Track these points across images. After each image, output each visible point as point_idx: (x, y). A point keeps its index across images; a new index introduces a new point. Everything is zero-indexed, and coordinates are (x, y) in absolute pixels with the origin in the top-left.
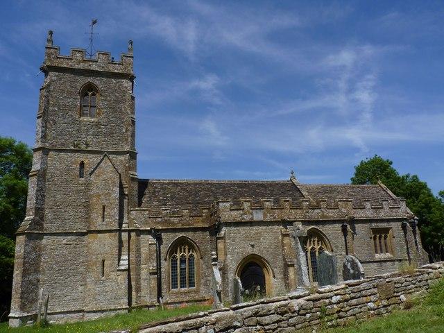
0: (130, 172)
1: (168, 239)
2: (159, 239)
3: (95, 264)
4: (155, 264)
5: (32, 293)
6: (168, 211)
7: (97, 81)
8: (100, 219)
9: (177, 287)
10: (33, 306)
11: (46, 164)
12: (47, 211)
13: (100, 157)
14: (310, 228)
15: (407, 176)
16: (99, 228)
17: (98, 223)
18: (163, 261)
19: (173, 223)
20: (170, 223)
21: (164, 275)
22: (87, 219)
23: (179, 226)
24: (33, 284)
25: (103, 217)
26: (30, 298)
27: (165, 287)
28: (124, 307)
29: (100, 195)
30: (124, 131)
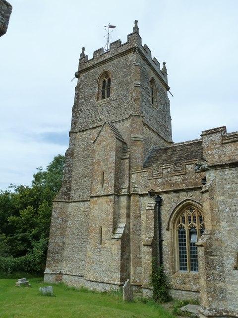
0: (132, 135)
1: (170, 203)
2: (159, 203)
3: (94, 230)
4: (152, 235)
5: (58, 253)
6: (169, 170)
7: (109, 67)
8: (100, 185)
9: (186, 269)
10: (59, 265)
11: (74, 144)
12: (73, 182)
13: (99, 129)
14: (132, 267)
15: (33, 182)
16: (98, 194)
17: (98, 189)
18: (164, 232)
19: (175, 184)
20: (171, 184)
21: (166, 250)
22: (91, 189)
23: (183, 187)
24: (59, 246)
25: (103, 183)
26: (56, 258)
27: (168, 265)
28: (116, 283)
29: (100, 162)
30: (130, 99)
